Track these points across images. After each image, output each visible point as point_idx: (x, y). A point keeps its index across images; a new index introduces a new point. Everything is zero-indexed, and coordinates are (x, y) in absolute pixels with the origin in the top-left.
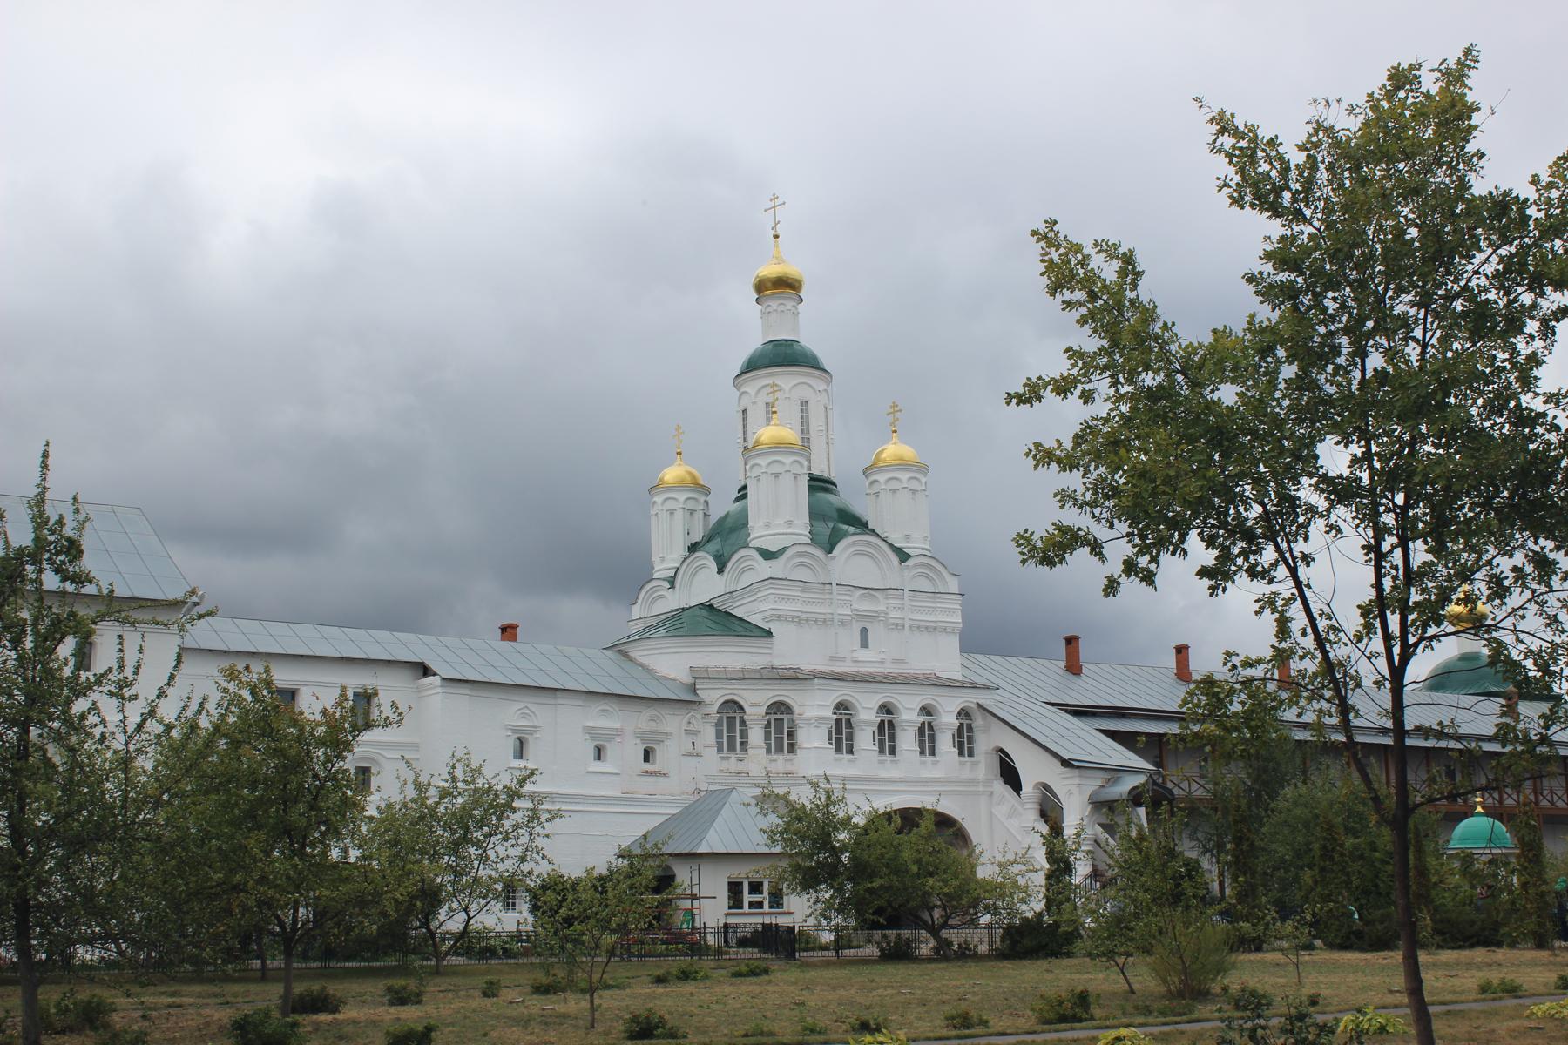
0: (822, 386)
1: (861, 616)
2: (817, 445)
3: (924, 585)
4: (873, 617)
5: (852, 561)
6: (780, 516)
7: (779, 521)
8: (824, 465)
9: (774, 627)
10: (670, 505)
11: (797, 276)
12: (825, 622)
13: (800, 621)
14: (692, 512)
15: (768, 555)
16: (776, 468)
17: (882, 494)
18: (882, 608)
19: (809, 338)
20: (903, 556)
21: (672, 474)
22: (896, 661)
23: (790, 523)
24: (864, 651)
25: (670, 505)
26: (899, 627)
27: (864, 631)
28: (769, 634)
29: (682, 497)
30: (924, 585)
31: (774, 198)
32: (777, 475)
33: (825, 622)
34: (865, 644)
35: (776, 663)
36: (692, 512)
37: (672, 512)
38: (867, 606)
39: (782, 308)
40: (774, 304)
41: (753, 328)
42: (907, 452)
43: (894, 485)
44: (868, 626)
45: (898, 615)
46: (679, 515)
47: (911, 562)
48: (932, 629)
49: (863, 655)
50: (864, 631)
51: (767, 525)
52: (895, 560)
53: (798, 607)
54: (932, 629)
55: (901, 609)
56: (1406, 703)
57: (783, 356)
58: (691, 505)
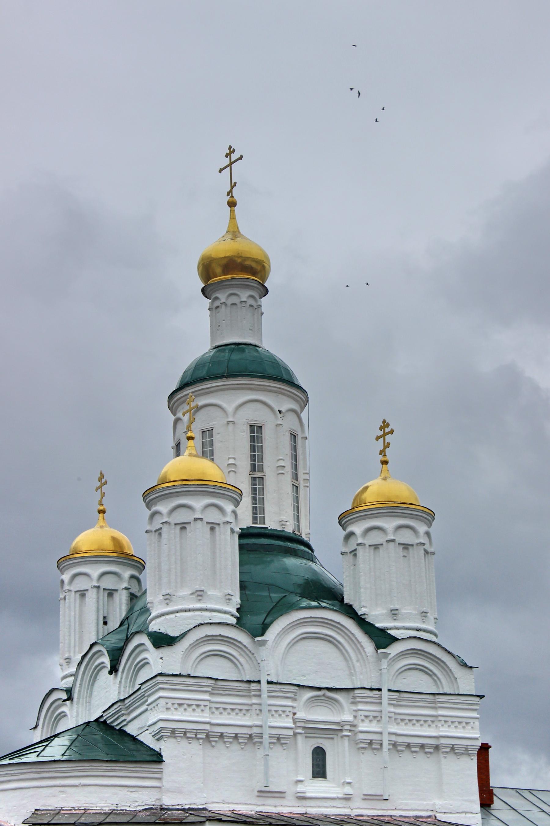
0: (287, 404)
1: (310, 730)
2: (277, 488)
3: (420, 682)
4: (334, 731)
5: (296, 648)
6: (198, 584)
7: (186, 592)
8: (288, 516)
9: (166, 748)
10: (81, 584)
11: (255, 254)
12: (252, 739)
13: (209, 737)
14: (111, 593)
15: (162, 641)
16: (182, 516)
17: (361, 552)
18: (347, 717)
19: (273, 342)
20: (382, 638)
21: (89, 538)
22: (368, 798)
23: (200, 594)
24: (319, 783)
25: (81, 584)
26: (373, 745)
27: (319, 755)
28: (157, 758)
29: (95, 571)
30: (420, 682)
31: (231, 151)
32: (183, 527)
33: (252, 739)
34: (319, 770)
35: (168, 801)
36: (111, 593)
37: (83, 594)
38: (322, 715)
39: (234, 300)
40: (222, 296)
41: (194, 333)
42: (398, 489)
43: (375, 538)
44: (327, 745)
45: (374, 727)
46: (91, 595)
47: (394, 650)
48: (434, 749)
49: (316, 788)
50: (319, 755)
51: (168, 598)
52: (368, 646)
53: (205, 717)
54: (434, 749)
55: (377, 718)
56: (289, 529)
57: (236, 364)
58: (108, 583)
